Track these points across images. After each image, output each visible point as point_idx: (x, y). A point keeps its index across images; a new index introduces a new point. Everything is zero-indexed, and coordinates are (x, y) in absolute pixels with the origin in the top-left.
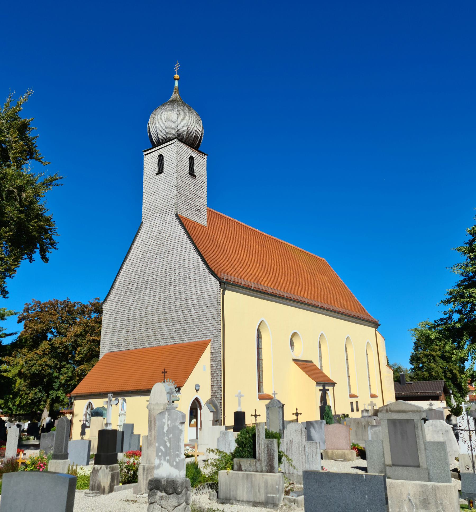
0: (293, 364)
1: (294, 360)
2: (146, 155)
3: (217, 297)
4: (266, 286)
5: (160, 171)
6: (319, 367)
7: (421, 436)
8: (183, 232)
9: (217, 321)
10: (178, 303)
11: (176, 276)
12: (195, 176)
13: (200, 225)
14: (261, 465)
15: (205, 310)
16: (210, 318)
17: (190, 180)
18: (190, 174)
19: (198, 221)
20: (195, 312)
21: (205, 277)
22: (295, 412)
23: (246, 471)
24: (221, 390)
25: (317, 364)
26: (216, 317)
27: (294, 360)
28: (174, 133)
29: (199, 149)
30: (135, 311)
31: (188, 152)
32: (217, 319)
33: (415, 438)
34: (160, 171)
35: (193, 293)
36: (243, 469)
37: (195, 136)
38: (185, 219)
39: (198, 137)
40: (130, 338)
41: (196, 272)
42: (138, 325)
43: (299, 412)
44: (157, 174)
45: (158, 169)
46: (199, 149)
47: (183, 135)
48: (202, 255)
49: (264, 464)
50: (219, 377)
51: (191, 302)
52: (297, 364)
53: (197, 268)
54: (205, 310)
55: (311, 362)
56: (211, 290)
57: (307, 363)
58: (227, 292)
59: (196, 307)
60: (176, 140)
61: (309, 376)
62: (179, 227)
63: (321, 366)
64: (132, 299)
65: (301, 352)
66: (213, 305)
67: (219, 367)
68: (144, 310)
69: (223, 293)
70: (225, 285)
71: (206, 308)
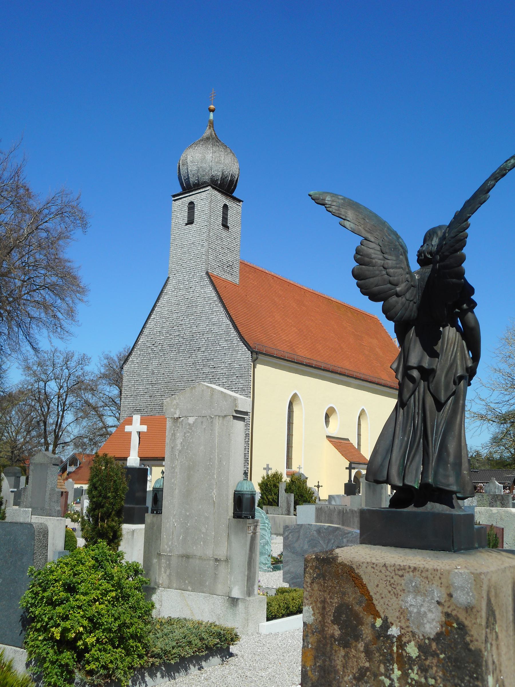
0: (327, 443)
1: (328, 437)
2: (175, 200)
3: (247, 368)
4: (303, 353)
5: (190, 222)
6: (356, 446)
7: (384, 493)
8: (214, 294)
9: (247, 393)
10: (207, 370)
11: (204, 341)
12: (228, 227)
13: (231, 283)
14: (282, 510)
15: (234, 380)
16: (240, 389)
17: (224, 233)
18: (223, 225)
19: (229, 278)
20: (224, 381)
21: (235, 344)
22: (317, 485)
23: (271, 514)
24: (248, 463)
25: (354, 442)
26: (246, 389)
27: (328, 437)
28: (207, 178)
29: (235, 194)
30: (159, 375)
31: (221, 199)
32: (247, 391)
33: (381, 494)
34: (190, 222)
35: (223, 361)
36: (269, 513)
37: (230, 180)
38: (216, 277)
39: (235, 177)
40: (153, 403)
41: (226, 339)
42: (163, 390)
43: (320, 485)
44: (187, 224)
45: (188, 218)
46: (235, 194)
47: (217, 180)
48: (233, 320)
49: (284, 510)
50: (247, 450)
51: (219, 371)
52: (330, 441)
53: (228, 333)
54: (234, 380)
55: (347, 440)
56: (242, 359)
57: (342, 441)
58: (258, 366)
59: (225, 376)
60: (209, 187)
61: (342, 455)
62: (210, 289)
63: (359, 444)
64: (155, 362)
65: (335, 428)
66: (243, 375)
67: (247, 440)
68: (168, 374)
69: (254, 367)
70: (258, 354)
71: (235, 378)
